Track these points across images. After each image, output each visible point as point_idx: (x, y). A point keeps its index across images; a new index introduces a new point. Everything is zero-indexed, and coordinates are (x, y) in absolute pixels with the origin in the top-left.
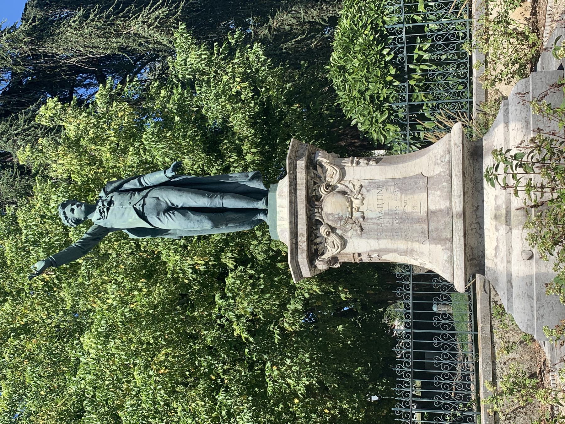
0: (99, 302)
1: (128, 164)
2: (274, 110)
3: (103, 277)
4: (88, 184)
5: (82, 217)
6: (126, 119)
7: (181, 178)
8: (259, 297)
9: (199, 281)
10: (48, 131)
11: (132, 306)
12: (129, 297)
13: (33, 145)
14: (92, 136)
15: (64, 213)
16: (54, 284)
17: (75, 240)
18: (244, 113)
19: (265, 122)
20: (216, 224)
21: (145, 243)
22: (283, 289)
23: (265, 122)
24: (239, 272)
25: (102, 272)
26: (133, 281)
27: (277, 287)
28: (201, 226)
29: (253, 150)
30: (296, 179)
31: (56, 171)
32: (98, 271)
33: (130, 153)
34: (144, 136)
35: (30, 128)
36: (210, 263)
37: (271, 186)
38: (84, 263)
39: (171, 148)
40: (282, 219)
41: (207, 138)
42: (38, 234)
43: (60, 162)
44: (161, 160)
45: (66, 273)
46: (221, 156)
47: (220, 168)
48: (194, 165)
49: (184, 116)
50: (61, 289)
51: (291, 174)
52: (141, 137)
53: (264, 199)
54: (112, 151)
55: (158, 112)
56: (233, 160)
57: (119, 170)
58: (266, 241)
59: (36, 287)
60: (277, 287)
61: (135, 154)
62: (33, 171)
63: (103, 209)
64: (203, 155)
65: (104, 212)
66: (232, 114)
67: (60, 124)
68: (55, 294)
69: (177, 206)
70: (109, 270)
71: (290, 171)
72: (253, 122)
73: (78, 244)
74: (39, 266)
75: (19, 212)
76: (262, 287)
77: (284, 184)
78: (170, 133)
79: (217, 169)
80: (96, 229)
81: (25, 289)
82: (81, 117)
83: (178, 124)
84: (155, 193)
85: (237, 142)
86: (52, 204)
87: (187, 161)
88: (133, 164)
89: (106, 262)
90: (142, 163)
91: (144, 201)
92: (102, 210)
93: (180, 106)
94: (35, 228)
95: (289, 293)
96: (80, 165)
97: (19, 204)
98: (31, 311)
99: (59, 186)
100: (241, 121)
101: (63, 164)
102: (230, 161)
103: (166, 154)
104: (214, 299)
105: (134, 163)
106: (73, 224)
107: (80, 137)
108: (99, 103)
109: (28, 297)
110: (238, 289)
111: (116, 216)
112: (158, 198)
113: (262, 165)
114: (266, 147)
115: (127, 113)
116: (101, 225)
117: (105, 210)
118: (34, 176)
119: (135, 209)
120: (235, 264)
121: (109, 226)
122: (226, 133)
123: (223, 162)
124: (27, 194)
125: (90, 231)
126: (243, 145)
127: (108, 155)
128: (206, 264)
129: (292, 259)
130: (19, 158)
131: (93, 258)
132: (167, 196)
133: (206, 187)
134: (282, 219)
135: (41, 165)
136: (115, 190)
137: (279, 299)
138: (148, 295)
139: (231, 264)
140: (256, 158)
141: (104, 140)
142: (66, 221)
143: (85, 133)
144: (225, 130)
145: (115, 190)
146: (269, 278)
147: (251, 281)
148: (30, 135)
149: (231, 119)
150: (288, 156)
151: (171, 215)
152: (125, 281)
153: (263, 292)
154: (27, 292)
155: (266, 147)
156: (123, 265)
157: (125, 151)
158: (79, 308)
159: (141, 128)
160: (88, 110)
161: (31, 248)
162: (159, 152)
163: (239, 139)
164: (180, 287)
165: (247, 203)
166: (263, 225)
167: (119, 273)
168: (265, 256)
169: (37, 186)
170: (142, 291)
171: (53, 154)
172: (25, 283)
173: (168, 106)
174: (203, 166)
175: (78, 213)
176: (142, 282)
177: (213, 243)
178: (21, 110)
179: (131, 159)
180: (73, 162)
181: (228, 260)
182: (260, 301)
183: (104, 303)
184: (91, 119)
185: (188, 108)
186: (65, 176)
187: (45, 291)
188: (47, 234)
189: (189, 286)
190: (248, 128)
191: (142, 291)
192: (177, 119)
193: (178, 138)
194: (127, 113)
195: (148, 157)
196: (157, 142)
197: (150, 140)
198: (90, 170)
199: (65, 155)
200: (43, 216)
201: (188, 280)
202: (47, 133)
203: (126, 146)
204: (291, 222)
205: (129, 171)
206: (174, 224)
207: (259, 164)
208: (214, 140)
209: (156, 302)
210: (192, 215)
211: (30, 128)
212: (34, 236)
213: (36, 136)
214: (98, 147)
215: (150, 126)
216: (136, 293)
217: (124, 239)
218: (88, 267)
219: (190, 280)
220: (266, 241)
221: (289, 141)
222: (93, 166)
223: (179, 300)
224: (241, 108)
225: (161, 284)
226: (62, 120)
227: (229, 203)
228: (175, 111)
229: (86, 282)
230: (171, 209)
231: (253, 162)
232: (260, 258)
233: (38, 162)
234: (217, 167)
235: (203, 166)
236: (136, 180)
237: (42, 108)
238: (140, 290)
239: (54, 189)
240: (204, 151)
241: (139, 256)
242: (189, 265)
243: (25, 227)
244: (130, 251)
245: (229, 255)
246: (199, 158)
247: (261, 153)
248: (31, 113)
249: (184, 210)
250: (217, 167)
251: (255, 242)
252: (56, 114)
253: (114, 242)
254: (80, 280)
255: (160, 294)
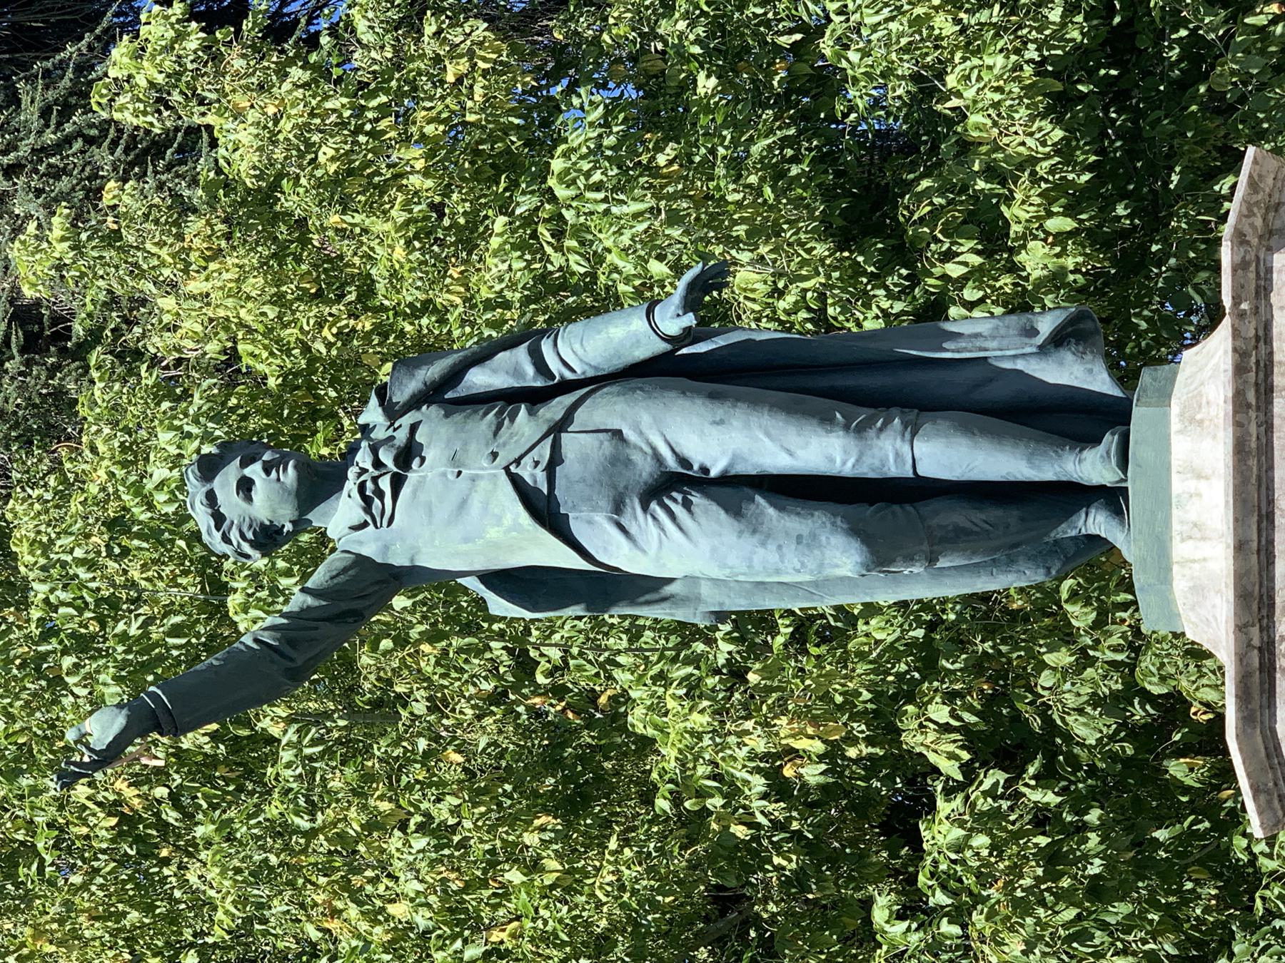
0: (353, 912)
1: (485, 294)
2: (1161, 35)
3: (372, 802)
4: (311, 387)
5: (285, 517)
6: (478, 92)
7: (720, 342)
8: (1079, 917)
9: (799, 832)
10: (143, 153)
11: (496, 936)
12: (486, 893)
13: (78, 217)
14: (332, 168)
15: (211, 498)
16: (163, 826)
17: (252, 623)
18: (1017, 51)
19: (1115, 93)
20: (882, 555)
21: (555, 654)
22: (1197, 882)
23: (1115, 93)
24: (986, 794)
25: (368, 777)
26: (500, 821)
27: (1169, 875)
28: (812, 565)
29: (1054, 224)
30: (1268, 340)
31: (176, 328)
32: (349, 771)
33: (495, 242)
34: (557, 165)
35: (68, 140)
36: (852, 753)
37: (1146, 376)
38: (291, 736)
39: (674, 218)
40: (1198, 531)
41: (838, 174)
42: (98, 602)
43: (196, 286)
44: (629, 268)
45: (210, 780)
46: (905, 253)
47: (898, 307)
48: (781, 294)
49: (737, 73)
50: (191, 849)
51: (1241, 315)
52: (545, 170)
53: (1110, 441)
54: (416, 237)
55: (619, 60)
56: (962, 270)
57: (442, 321)
58: (1116, 649)
59: (87, 837)
60: (1169, 875)
61: (515, 247)
62: (78, 329)
63: (375, 480)
64: (821, 249)
65: (380, 494)
66: (958, 55)
67: (197, 120)
68: (166, 872)
69: (705, 470)
70: (395, 769)
71: (1237, 300)
72: (1057, 90)
73: (267, 638)
74: (102, 728)
75: (19, 508)
76: (1095, 868)
77: (1207, 368)
78: (671, 150)
79: (886, 314)
80: (345, 570)
81: (40, 846)
82: (287, 86)
83: (707, 110)
84: (604, 411)
85: (981, 184)
86: (159, 472)
87: (748, 279)
88: (508, 294)
89: (383, 734)
90: (546, 286)
91: (556, 447)
92: (369, 485)
93: (718, 26)
94: (83, 574)
95: (1224, 901)
96: (278, 300)
97: (15, 475)
98: (60, 943)
99: (185, 391)
100: (998, 89)
101: (207, 297)
102: (945, 277)
103: (651, 245)
104: (868, 921)
105: (512, 286)
106: (246, 548)
107: (280, 176)
108: (361, 25)
109: (52, 883)
110: (979, 875)
111: (430, 513)
112: (617, 434)
113: (1100, 293)
114: (1120, 210)
115: (482, 65)
116: (366, 551)
117: (385, 484)
118: (83, 350)
119: (516, 481)
120: (966, 756)
121: (399, 559)
122: (934, 149)
123: (914, 279)
124: (52, 433)
125: (319, 577)
126: (1009, 200)
127: (399, 253)
128: (832, 754)
129: (1247, 719)
130: (22, 271)
131: (327, 715)
132: (657, 422)
133: (841, 381)
134: (1198, 531)
135: (113, 301)
136: (432, 395)
137: (1177, 929)
138: (568, 890)
139: (946, 759)
140: (1070, 262)
141: (382, 189)
142: (218, 535)
143: (301, 156)
144: (926, 132)
145: (432, 395)
146: (1129, 827)
147: (1043, 841)
148: (65, 171)
149: (951, 81)
150: (1227, 230)
151: (678, 509)
152: (468, 824)
153: (1098, 891)
154: (49, 859)
155: (1120, 210)
156: (458, 751)
157: (470, 237)
158: (266, 933)
159: (542, 131)
160: (313, 58)
161: (68, 662)
162: (622, 233)
163: (991, 172)
164: (711, 858)
165: (1029, 461)
166: (1103, 571)
167: (442, 784)
168: (1108, 724)
169: (96, 394)
170: (543, 870)
171: (164, 253)
172: (40, 820)
173: (664, 27)
174: (822, 298)
175: (269, 499)
176: (542, 829)
177: (862, 656)
178: (25, 66)
179: (500, 269)
180: (246, 288)
181: (932, 736)
182: (1083, 937)
183: (374, 917)
184: (326, 98)
185: (755, 34)
186: (212, 348)
187: (123, 861)
188: (136, 601)
189: (750, 856)
190: (1032, 118)
191: (543, 870)
192: (706, 84)
193: (706, 169)
194: (482, 65)
195: (573, 258)
196: (615, 190)
197: (581, 182)
198: (320, 325)
199: (217, 254)
200: (118, 525)
201: (749, 825)
202: (140, 161)
203: (475, 212)
204: (1240, 547)
205: (489, 324)
206: (690, 554)
207: (1081, 290)
208: (875, 180)
209: (604, 923)
210: (771, 511)
211: (68, 140)
212: (80, 611)
213: (94, 176)
214: (358, 218)
215: (585, 120)
216: (515, 876)
217: (461, 634)
218: (308, 751)
219: (758, 826)
220: (1116, 649)
221: (1230, 180)
222: (330, 303)
223: (707, 920)
224: (999, 30)
225: (625, 842)
226: (202, 102)
227: (945, 455)
228: (696, 50)
229: (297, 820)
230: (674, 484)
231: (1056, 279)
232: (1087, 730)
233: (97, 291)
234: (885, 304)
235: (822, 298)
236: (521, 353)
237: (120, 52)
238: (534, 867)
239: (166, 405)
240: (827, 230)
241: (531, 709)
242: (753, 756)
243: (44, 569)
244: (487, 686)
245: (940, 712)
246: (804, 263)
247: (1093, 238)
248: (70, 74)
249: (736, 490)
250: (885, 304)
251: (1062, 658)
252: (178, 75)
253: (418, 642)
254: (273, 810)
255: (622, 888)
